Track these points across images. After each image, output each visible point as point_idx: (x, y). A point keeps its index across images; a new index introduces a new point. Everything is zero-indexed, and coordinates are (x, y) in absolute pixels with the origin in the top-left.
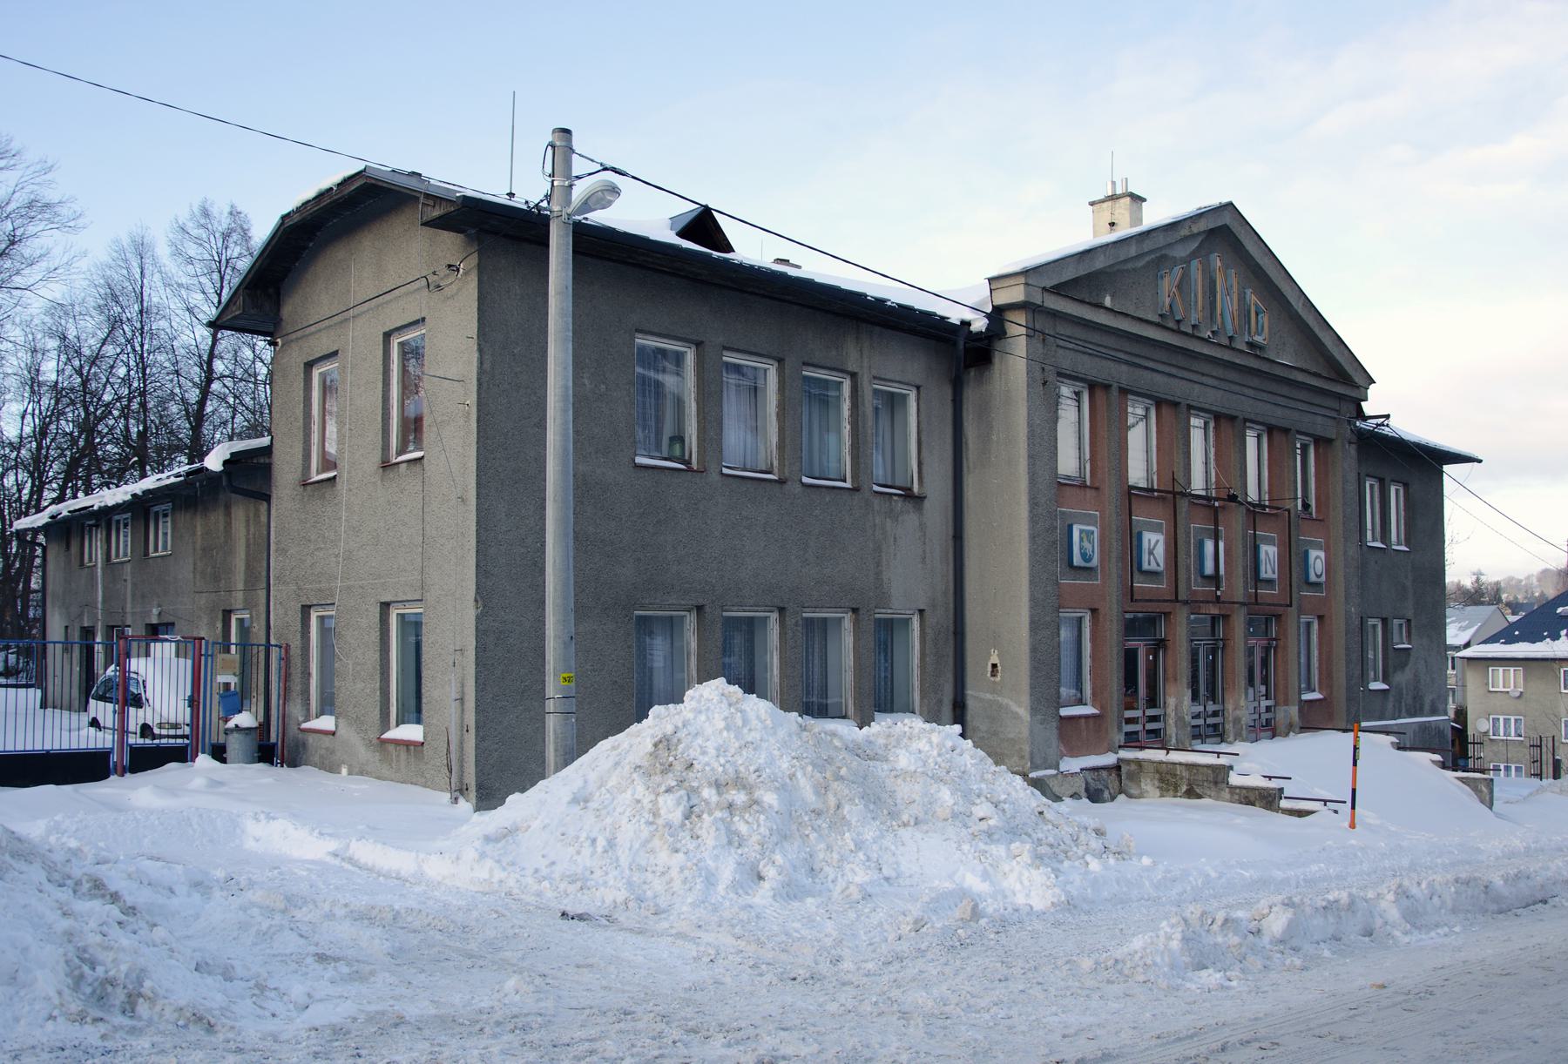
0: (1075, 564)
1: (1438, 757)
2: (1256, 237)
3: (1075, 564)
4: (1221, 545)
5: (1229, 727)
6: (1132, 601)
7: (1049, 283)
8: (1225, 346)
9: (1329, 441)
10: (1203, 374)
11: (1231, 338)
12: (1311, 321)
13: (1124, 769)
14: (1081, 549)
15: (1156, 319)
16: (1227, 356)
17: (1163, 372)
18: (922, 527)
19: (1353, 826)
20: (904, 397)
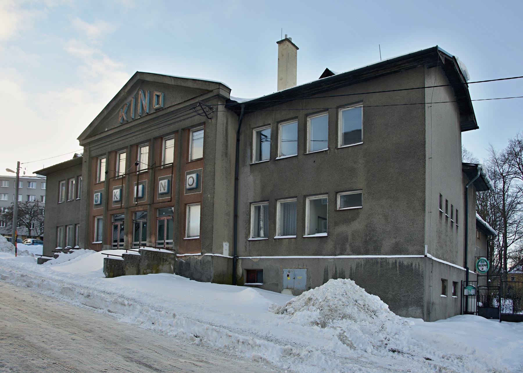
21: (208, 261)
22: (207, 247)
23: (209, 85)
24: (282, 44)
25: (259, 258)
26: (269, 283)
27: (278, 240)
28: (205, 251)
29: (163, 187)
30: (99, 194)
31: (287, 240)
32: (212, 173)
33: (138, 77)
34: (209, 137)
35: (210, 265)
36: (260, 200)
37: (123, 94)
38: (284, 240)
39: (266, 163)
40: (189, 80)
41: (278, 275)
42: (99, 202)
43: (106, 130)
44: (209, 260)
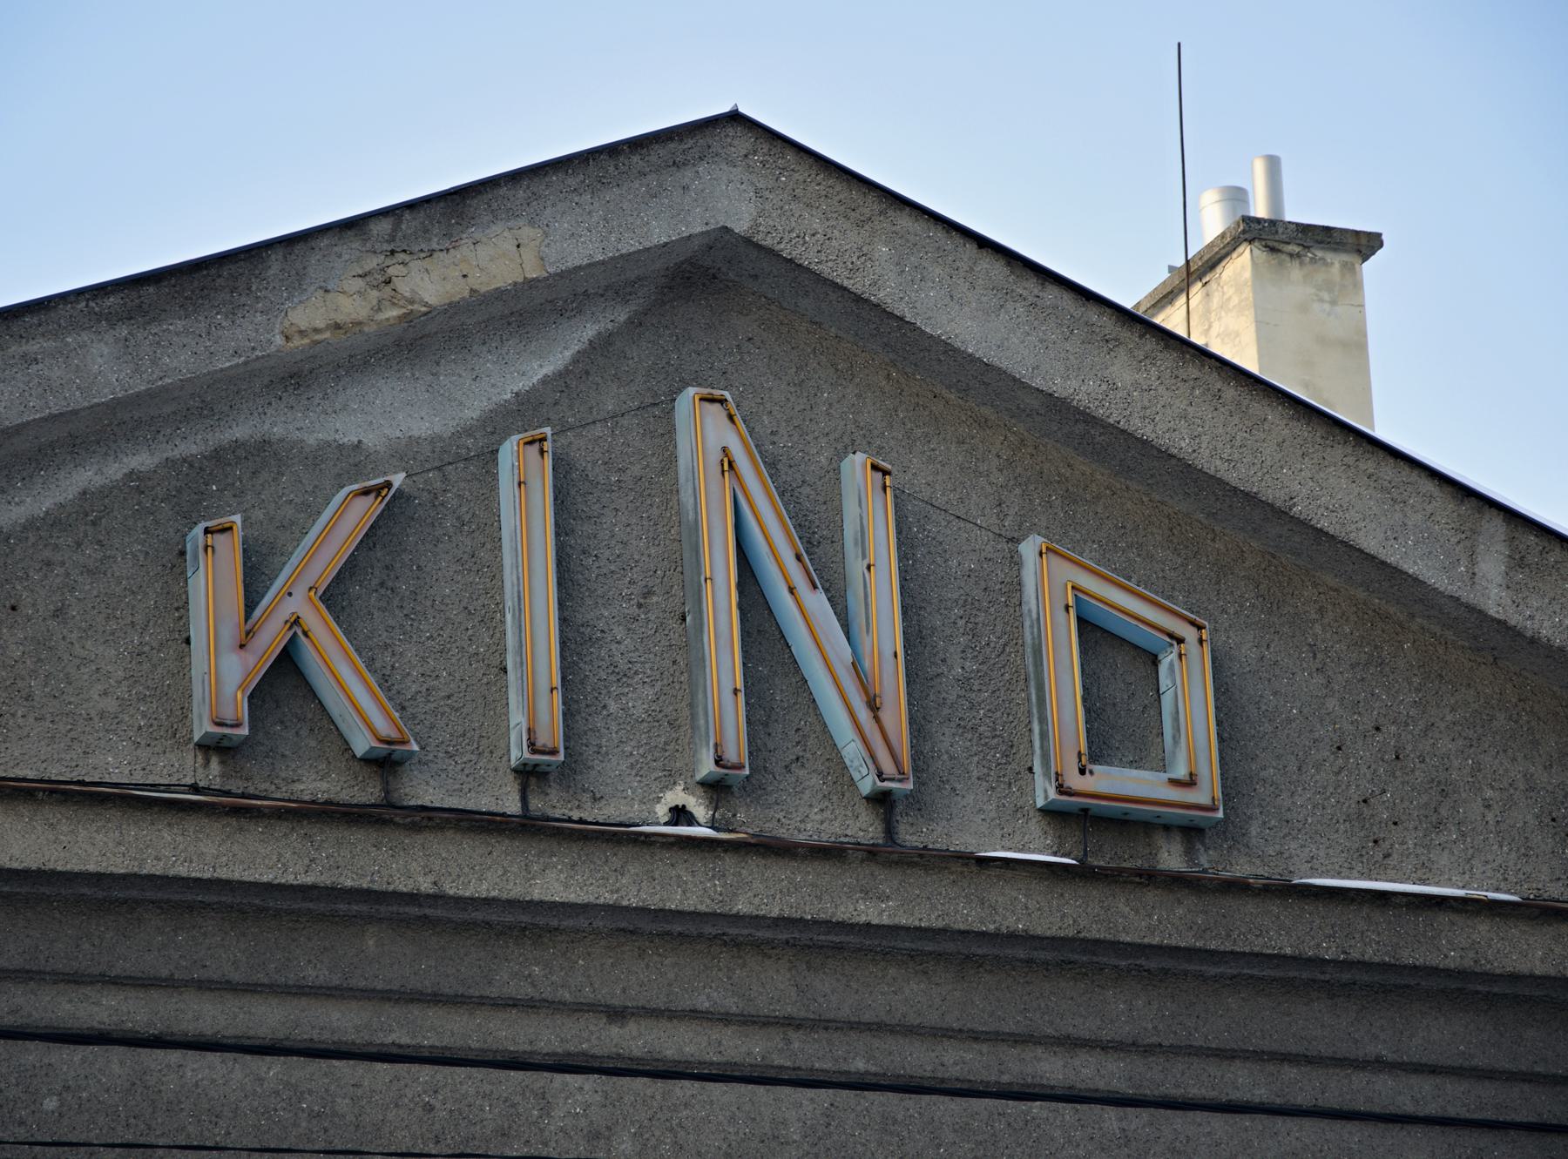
8: (871, 853)
10: (617, 1014)
11: (385, 763)
15: (864, 828)
24: (1295, 271)
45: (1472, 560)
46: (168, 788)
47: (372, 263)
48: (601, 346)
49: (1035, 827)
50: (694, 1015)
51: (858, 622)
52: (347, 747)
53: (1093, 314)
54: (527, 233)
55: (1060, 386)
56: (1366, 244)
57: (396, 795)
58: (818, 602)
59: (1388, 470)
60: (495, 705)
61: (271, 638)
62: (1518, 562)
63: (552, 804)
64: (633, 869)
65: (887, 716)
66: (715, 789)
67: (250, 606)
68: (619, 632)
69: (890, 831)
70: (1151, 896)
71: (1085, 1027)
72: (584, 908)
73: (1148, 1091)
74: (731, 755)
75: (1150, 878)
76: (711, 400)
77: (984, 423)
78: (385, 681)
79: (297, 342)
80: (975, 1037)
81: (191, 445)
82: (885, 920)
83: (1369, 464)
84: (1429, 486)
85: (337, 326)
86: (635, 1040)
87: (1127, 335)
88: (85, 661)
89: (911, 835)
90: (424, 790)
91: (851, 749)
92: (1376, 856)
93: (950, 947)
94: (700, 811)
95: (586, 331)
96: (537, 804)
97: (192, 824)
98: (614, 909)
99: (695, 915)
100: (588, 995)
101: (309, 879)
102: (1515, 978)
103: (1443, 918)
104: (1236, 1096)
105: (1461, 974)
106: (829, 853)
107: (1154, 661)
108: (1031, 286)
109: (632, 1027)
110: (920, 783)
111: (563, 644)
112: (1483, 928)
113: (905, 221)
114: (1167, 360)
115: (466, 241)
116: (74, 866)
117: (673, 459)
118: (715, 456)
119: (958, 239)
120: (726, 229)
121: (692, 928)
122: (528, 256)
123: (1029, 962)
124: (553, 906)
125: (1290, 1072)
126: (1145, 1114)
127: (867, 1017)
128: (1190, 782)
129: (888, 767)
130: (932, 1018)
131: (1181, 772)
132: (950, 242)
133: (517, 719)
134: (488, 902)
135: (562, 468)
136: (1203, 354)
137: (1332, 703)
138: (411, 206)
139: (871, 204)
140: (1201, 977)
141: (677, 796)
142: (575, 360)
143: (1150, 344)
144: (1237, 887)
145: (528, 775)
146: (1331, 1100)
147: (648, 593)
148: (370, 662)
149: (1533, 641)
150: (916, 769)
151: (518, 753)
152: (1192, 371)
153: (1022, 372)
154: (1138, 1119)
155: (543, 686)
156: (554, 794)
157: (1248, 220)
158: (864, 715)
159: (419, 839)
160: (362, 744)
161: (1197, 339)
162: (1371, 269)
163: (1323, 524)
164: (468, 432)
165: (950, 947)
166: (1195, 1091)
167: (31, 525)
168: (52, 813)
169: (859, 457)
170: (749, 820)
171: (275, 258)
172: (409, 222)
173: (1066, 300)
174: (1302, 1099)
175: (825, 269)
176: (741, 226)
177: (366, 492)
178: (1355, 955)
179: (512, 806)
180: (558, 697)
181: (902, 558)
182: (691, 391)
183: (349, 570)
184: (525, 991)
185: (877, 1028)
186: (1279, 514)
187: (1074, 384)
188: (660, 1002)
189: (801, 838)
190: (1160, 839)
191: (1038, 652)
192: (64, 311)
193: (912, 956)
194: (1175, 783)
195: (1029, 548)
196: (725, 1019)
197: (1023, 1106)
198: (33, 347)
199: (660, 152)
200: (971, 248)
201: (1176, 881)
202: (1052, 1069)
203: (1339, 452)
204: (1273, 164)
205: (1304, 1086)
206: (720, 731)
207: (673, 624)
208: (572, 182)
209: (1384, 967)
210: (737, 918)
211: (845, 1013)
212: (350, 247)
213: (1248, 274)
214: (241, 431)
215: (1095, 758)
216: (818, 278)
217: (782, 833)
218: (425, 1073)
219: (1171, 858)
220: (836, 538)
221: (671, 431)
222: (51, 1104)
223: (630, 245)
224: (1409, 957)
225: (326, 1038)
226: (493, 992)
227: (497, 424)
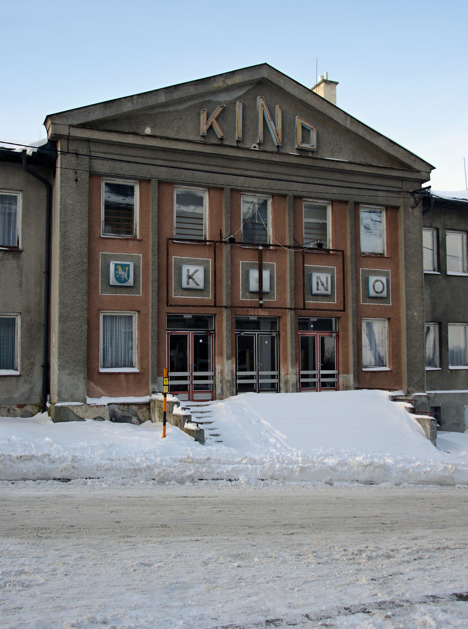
0: (111, 284)
1: (410, 405)
2: (294, 83)
3: (111, 284)
4: (266, 274)
5: (282, 385)
6: (167, 306)
7: (75, 122)
8: (276, 153)
9: (396, 208)
10: (246, 170)
11: (222, 139)
12: (361, 132)
13: (152, 404)
14: (116, 275)
15: (275, 150)
16: (264, 157)
17: (384, 190)
18: (20, 268)
19: (164, 436)
20: (15, 198)
21: (423, 403)
22: (416, 383)
23: (415, 161)
24: (329, 86)
25: (434, 394)
26: (448, 424)
27: (454, 371)
28: (414, 389)
29: (323, 285)
30: (132, 265)
31: (464, 371)
32: (418, 284)
33: (264, 74)
34: (410, 232)
35: (426, 408)
36: (431, 320)
37: (219, 84)
38: (461, 371)
39: (436, 276)
40: (383, 138)
41: (459, 412)
42: (131, 282)
43: (148, 131)
44: (424, 402)
45: (346, 121)
46: (197, 141)
47: (223, 79)
48: (249, 91)
49: (295, 150)
50: (255, 170)
51: (276, 125)
52: (217, 137)
53: (305, 90)
54: (241, 76)
55: (301, 98)
56: (337, 83)
57: (438, 619)
58: (272, 122)
59: (338, 110)
60: (234, 133)
61: (209, 124)
62: (351, 122)
63: (240, 145)
64: (249, 153)
65: (279, 136)
66: (259, 144)
67: (207, 120)
68: (249, 125)
69: (279, 150)
70: (308, 159)
71: (299, 174)
72: (243, 157)
73: (305, 182)
74: (261, 140)
75: (308, 157)
76: (261, 98)
77: (292, 102)
78: (222, 129)
79: (214, 88)
80: (287, 175)
81: (202, 100)
82: (277, 161)
83: (336, 109)
84: (342, 112)
85: (219, 87)
86: (248, 173)
87: (309, 92)
88: (188, 125)
89: (281, 151)
90: (226, 143)
91: (275, 140)
92: (333, 155)
93: (285, 164)
94: (257, 147)
95: (247, 89)
96: (239, 145)
97: (200, 145)
98: (247, 158)
99: (256, 159)
100: (243, 168)
101: (212, 152)
102: (347, 170)
103: (340, 163)
104: (315, 183)
105: (341, 170)
106: (272, 152)
107: (310, 132)
108: (299, 86)
109: (248, 172)
110: (282, 145)
111: (242, 126)
112: (344, 164)
113: (285, 77)
114: (314, 96)
115: (234, 77)
116: (187, 149)
117: (256, 104)
118: (261, 104)
119: (290, 80)
120: (264, 77)
121: (255, 160)
122: (241, 79)
123: (293, 166)
124: (240, 157)
125: (321, 180)
126: (305, 184)
127: (275, 172)
128: (313, 146)
129: (279, 143)
130: (282, 172)
131: (312, 145)
132: (290, 80)
133: (237, 135)
134: (233, 156)
135: (243, 105)
136: (318, 95)
137: (329, 137)
138: (228, 73)
139: (281, 75)
140: (312, 169)
141: (254, 145)
142: (246, 92)
143: (312, 93)
144: (317, 159)
145: (238, 141)
146: (326, 183)
147: (253, 120)
148: (220, 127)
149: (352, 131)
150: (282, 143)
151: (237, 139)
152: (316, 97)
153: (297, 96)
154: (304, 185)
155: (240, 131)
156: (241, 144)
157: (324, 80)
158: (276, 136)
159: (225, 148)
160: (219, 137)
161: (317, 93)
162: (337, 86)
163: (330, 116)
164: (233, 100)
165: (285, 164)
166: (311, 182)
167: (183, 109)
168: (184, 143)
169: (278, 105)
170: (263, 148)
171: (212, 78)
172: (228, 75)
173: (302, 88)
174: (322, 183)
175: (275, 82)
176: (266, 77)
177: (221, 107)
178: (330, 167)
179: (236, 145)
180: (241, 132)
181: (282, 118)
182: (259, 96)
183: (219, 116)
184: (236, 167)
185: (276, 173)
186: (325, 115)
187: (303, 98)
188: (251, 169)
189: (268, 150)
190: (309, 153)
191: (297, 130)
192: (188, 84)
193: (280, 165)
194: (311, 146)
195: (297, 117)
196: (259, 171)
197: (292, 183)
198: (184, 88)
199: (257, 67)
200: (292, 81)
201: (311, 158)
202: (295, 179)
203: (332, 108)
204: (327, 73)
205: (323, 182)
206: (260, 137)
207: (255, 124)
208: (246, 70)
209: (333, 169)
210: (260, 160)
211: (272, 171)
212: (221, 77)
213: (323, 86)
214: (207, 99)
215: (302, 143)
216: (274, 83)
217: (266, 150)
218: (225, 175)
219: (310, 155)
220: (274, 115)
221: (256, 101)
222: (183, 176)
223: (253, 78)
224: (336, 168)
225: (214, 171)
226: (232, 167)
227: (236, 99)
